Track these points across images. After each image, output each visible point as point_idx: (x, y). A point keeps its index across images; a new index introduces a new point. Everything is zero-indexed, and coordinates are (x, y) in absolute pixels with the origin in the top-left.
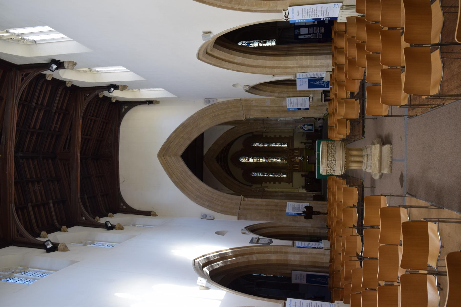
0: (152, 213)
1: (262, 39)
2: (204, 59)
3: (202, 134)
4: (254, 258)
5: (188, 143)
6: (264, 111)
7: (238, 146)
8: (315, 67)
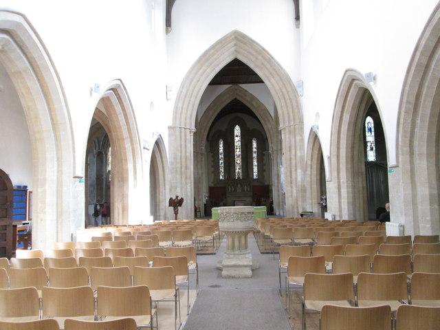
0: (169, 29)
1: (376, 146)
2: (345, 78)
3: (262, 82)
4: (128, 145)
5: (252, 66)
6: (290, 150)
7: (251, 124)
8: (340, 202)
